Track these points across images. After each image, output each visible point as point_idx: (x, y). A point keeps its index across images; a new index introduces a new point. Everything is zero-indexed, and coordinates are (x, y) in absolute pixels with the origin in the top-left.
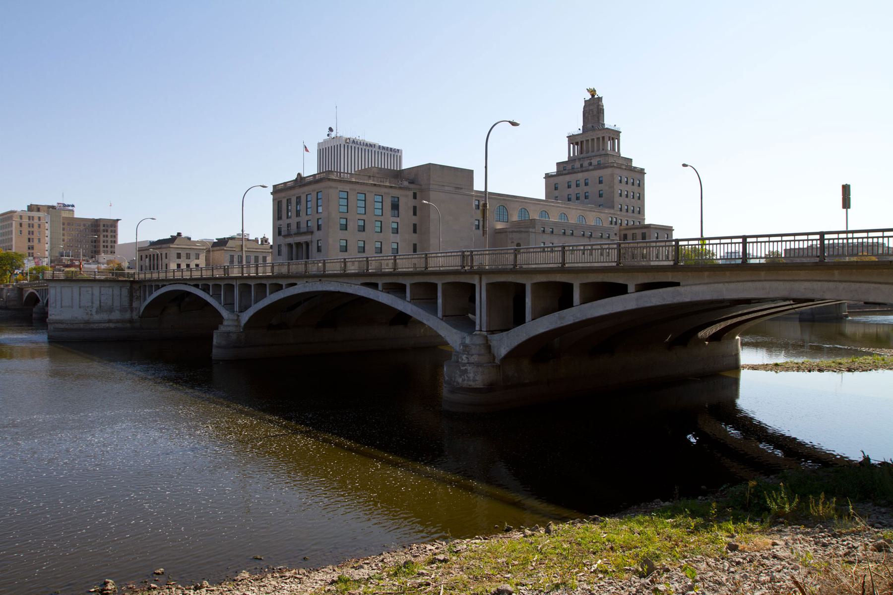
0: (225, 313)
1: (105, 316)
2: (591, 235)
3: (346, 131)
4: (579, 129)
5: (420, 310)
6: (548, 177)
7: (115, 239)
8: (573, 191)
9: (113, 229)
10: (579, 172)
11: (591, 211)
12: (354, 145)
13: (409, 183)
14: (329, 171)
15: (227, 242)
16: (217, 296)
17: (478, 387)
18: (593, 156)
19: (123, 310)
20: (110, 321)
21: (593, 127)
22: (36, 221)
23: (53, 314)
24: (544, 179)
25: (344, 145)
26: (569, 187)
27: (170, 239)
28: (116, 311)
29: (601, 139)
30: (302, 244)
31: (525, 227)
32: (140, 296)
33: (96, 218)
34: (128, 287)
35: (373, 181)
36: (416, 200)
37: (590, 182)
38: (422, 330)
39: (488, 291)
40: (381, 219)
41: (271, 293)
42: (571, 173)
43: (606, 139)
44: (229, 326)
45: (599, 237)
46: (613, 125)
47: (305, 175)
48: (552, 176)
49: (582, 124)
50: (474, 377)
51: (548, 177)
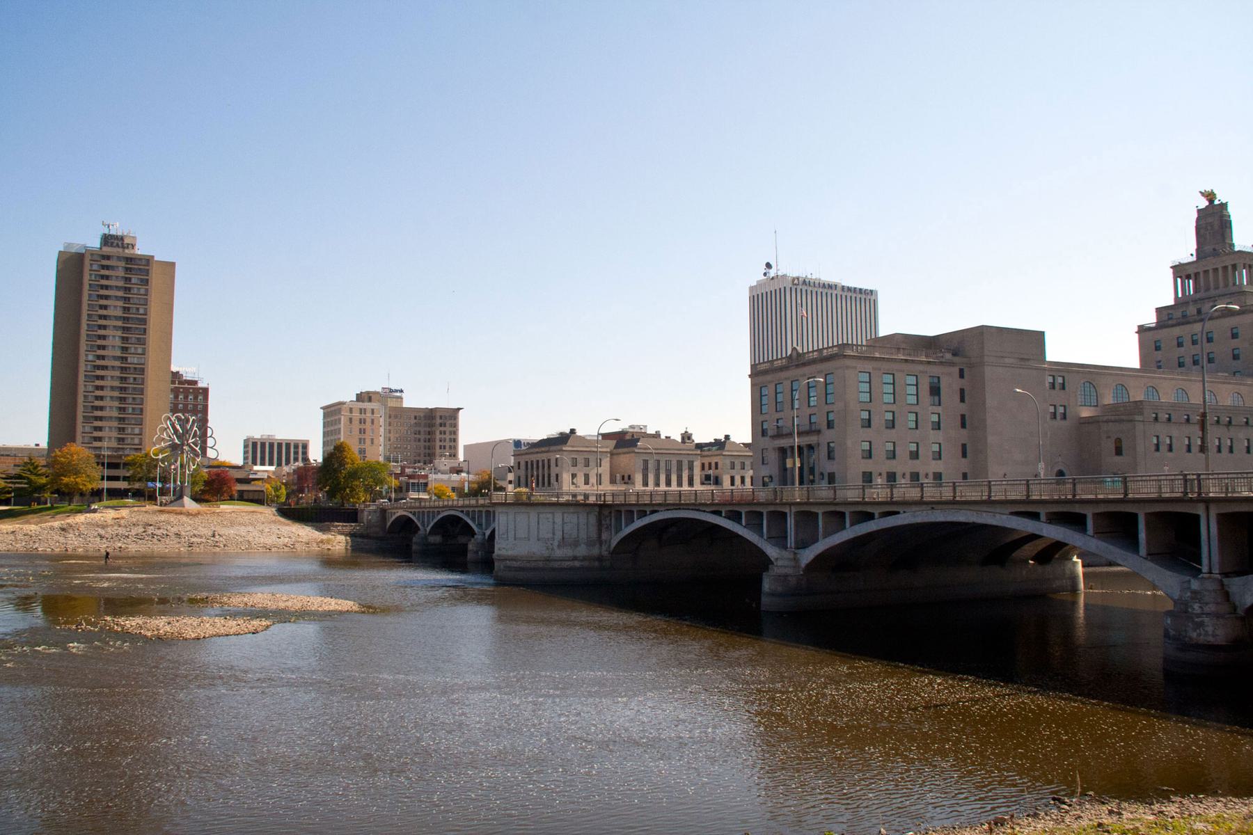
0: (772, 551)
1: (568, 552)
2: (1230, 422)
3: (791, 267)
4: (1192, 255)
5: (1111, 547)
6: (1142, 330)
7: (454, 437)
8: (1188, 351)
9: (452, 421)
10: (1195, 322)
11: (1224, 383)
12: (804, 288)
13: (953, 355)
14: (843, 344)
15: (638, 440)
17: (1220, 643)
18: (1219, 296)
19: (590, 544)
20: (575, 558)
21: (1214, 250)
22: (369, 414)
23: (504, 548)
24: (1137, 335)
25: (791, 288)
26: (1180, 345)
27: (558, 438)
28: (582, 545)
29: (1230, 268)
31: (1127, 413)
32: (610, 525)
33: (430, 407)
34: (596, 513)
35: (903, 355)
36: (963, 380)
37: (1215, 337)
38: (1024, 572)
39: (1219, 523)
40: (916, 409)
41: (852, 524)
42: (1183, 324)
43: (1240, 266)
44: (785, 567)
45: (1243, 423)
48: (1150, 329)
49: (1195, 247)
50: (1213, 631)
51: (1142, 330)
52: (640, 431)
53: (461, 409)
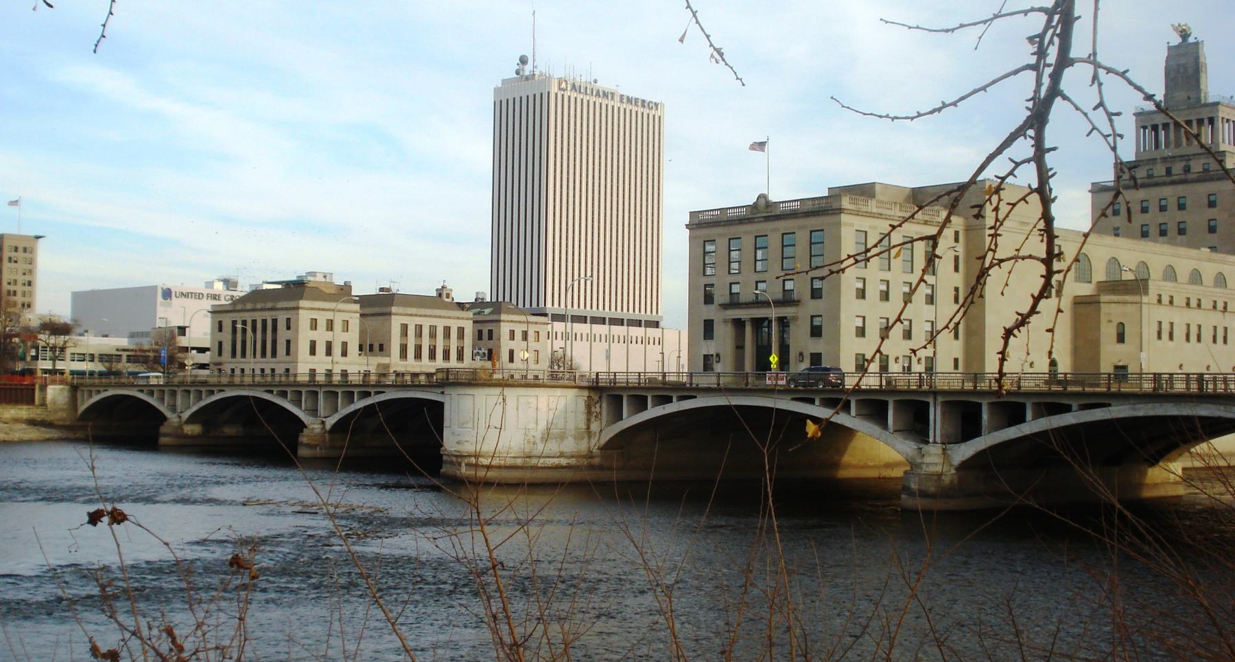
1: (553, 447)
16: (298, 403)
18: (1194, 155)
20: (562, 455)
24: (1090, 194)
25: (556, 94)
30: (770, 322)
37: (1188, 203)
41: (207, 396)
46: (1229, 97)
47: (773, 198)
51: (1097, 189)
52: (324, 280)
53: (40, 237)
